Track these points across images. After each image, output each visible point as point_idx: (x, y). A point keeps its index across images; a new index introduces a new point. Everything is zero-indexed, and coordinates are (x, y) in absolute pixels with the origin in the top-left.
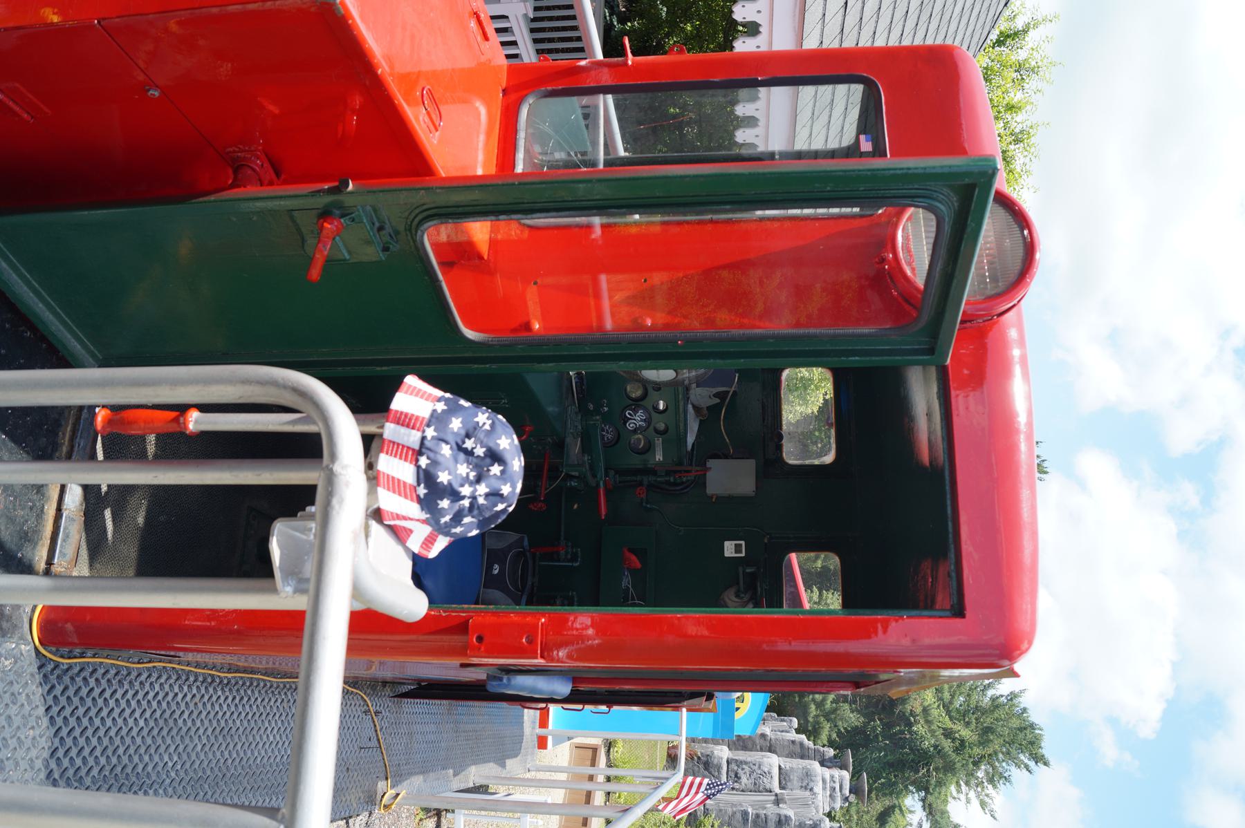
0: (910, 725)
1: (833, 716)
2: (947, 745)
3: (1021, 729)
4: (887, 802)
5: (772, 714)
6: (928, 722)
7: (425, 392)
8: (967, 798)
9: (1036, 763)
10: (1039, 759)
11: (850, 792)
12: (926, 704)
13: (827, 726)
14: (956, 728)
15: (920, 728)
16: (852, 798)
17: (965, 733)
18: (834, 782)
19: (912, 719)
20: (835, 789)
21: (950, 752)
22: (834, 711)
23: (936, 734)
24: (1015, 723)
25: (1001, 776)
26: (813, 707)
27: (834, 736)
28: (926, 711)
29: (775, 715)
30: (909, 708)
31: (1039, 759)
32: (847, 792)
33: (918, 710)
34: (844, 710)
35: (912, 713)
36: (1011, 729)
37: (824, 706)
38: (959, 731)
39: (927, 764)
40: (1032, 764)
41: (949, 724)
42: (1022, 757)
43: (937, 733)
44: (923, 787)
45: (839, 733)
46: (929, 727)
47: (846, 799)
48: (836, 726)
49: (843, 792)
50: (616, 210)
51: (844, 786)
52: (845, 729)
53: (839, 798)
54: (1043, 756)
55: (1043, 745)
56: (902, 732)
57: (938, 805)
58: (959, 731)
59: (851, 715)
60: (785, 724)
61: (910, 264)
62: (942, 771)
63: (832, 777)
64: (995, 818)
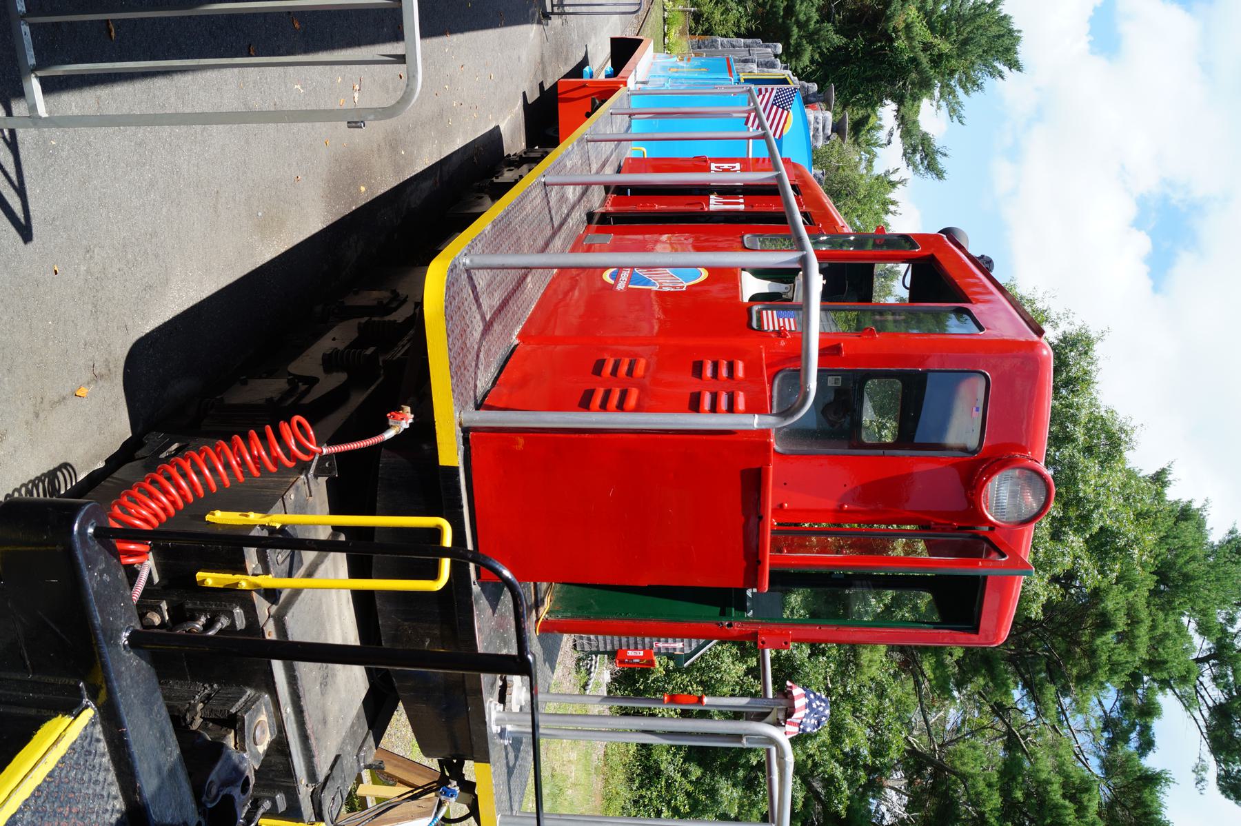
0: (891, 40)
1: (816, 37)
2: (924, 60)
3: (999, 36)
4: (862, 113)
5: (757, 40)
6: (910, 39)
7: (604, 407)
8: (938, 105)
9: (1010, 68)
10: (1014, 65)
11: (832, 131)
12: (910, 20)
13: (809, 49)
14: (936, 41)
15: (900, 43)
16: (835, 136)
17: (945, 47)
18: (818, 123)
19: (894, 35)
20: (818, 129)
21: (927, 69)
22: (817, 31)
23: (916, 50)
24: (994, 30)
25: (974, 83)
26: (795, 30)
27: (817, 56)
28: (908, 27)
29: (760, 41)
30: (891, 25)
31: (1014, 65)
32: (829, 132)
33: (901, 26)
34: (827, 31)
35: (895, 30)
36: (989, 37)
37: (808, 26)
38: (939, 45)
39: (903, 79)
40: (1005, 69)
41: (930, 39)
42: (996, 64)
43: (917, 50)
44: (900, 100)
45: (821, 54)
46: (911, 43)
47: (828, 138)
48: (819, 47)
49: (826, 132)
50: (812, 563)
51: (827, 127)
52: (828, 49)
53: (821, 138)
54: (1018, 61)
55: (1015, 27)
56: (882, 48)
57: (910, 116)
58: (939, 45)
59: (834, 37)
60: (770, 50)
61: (985, 504)
62: (918, 86)
63: (816, 118)
64: (963, 124)
